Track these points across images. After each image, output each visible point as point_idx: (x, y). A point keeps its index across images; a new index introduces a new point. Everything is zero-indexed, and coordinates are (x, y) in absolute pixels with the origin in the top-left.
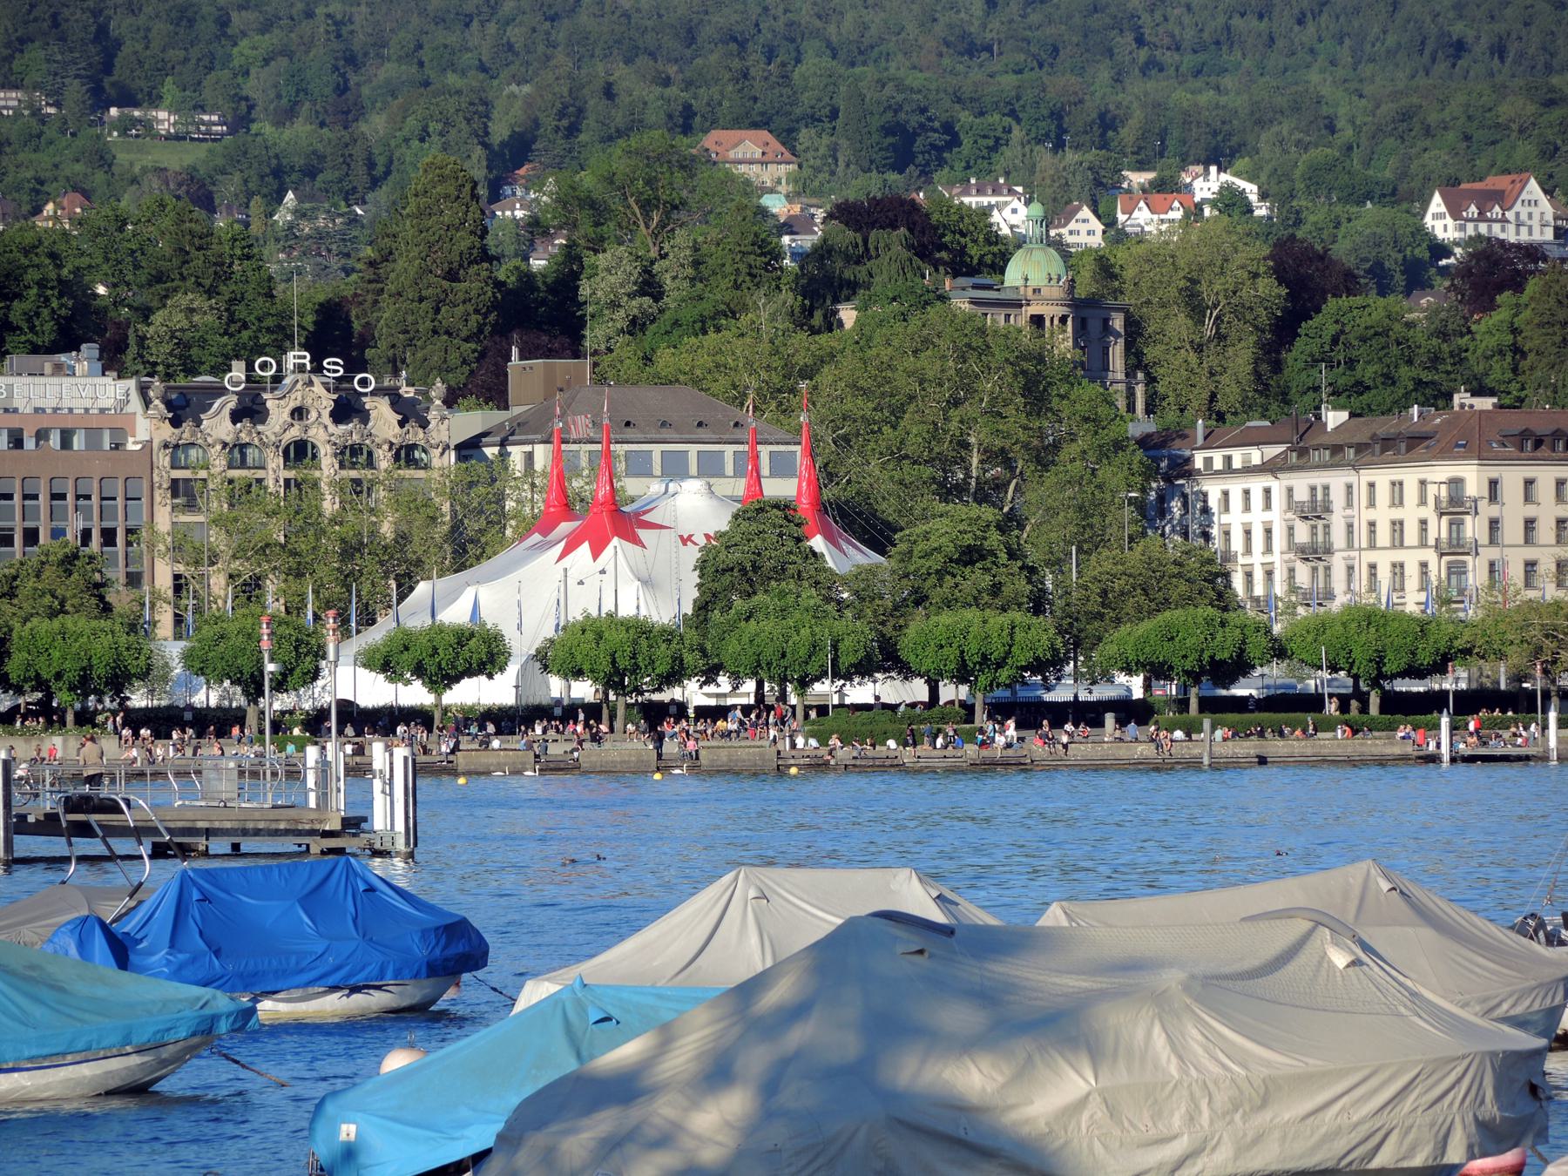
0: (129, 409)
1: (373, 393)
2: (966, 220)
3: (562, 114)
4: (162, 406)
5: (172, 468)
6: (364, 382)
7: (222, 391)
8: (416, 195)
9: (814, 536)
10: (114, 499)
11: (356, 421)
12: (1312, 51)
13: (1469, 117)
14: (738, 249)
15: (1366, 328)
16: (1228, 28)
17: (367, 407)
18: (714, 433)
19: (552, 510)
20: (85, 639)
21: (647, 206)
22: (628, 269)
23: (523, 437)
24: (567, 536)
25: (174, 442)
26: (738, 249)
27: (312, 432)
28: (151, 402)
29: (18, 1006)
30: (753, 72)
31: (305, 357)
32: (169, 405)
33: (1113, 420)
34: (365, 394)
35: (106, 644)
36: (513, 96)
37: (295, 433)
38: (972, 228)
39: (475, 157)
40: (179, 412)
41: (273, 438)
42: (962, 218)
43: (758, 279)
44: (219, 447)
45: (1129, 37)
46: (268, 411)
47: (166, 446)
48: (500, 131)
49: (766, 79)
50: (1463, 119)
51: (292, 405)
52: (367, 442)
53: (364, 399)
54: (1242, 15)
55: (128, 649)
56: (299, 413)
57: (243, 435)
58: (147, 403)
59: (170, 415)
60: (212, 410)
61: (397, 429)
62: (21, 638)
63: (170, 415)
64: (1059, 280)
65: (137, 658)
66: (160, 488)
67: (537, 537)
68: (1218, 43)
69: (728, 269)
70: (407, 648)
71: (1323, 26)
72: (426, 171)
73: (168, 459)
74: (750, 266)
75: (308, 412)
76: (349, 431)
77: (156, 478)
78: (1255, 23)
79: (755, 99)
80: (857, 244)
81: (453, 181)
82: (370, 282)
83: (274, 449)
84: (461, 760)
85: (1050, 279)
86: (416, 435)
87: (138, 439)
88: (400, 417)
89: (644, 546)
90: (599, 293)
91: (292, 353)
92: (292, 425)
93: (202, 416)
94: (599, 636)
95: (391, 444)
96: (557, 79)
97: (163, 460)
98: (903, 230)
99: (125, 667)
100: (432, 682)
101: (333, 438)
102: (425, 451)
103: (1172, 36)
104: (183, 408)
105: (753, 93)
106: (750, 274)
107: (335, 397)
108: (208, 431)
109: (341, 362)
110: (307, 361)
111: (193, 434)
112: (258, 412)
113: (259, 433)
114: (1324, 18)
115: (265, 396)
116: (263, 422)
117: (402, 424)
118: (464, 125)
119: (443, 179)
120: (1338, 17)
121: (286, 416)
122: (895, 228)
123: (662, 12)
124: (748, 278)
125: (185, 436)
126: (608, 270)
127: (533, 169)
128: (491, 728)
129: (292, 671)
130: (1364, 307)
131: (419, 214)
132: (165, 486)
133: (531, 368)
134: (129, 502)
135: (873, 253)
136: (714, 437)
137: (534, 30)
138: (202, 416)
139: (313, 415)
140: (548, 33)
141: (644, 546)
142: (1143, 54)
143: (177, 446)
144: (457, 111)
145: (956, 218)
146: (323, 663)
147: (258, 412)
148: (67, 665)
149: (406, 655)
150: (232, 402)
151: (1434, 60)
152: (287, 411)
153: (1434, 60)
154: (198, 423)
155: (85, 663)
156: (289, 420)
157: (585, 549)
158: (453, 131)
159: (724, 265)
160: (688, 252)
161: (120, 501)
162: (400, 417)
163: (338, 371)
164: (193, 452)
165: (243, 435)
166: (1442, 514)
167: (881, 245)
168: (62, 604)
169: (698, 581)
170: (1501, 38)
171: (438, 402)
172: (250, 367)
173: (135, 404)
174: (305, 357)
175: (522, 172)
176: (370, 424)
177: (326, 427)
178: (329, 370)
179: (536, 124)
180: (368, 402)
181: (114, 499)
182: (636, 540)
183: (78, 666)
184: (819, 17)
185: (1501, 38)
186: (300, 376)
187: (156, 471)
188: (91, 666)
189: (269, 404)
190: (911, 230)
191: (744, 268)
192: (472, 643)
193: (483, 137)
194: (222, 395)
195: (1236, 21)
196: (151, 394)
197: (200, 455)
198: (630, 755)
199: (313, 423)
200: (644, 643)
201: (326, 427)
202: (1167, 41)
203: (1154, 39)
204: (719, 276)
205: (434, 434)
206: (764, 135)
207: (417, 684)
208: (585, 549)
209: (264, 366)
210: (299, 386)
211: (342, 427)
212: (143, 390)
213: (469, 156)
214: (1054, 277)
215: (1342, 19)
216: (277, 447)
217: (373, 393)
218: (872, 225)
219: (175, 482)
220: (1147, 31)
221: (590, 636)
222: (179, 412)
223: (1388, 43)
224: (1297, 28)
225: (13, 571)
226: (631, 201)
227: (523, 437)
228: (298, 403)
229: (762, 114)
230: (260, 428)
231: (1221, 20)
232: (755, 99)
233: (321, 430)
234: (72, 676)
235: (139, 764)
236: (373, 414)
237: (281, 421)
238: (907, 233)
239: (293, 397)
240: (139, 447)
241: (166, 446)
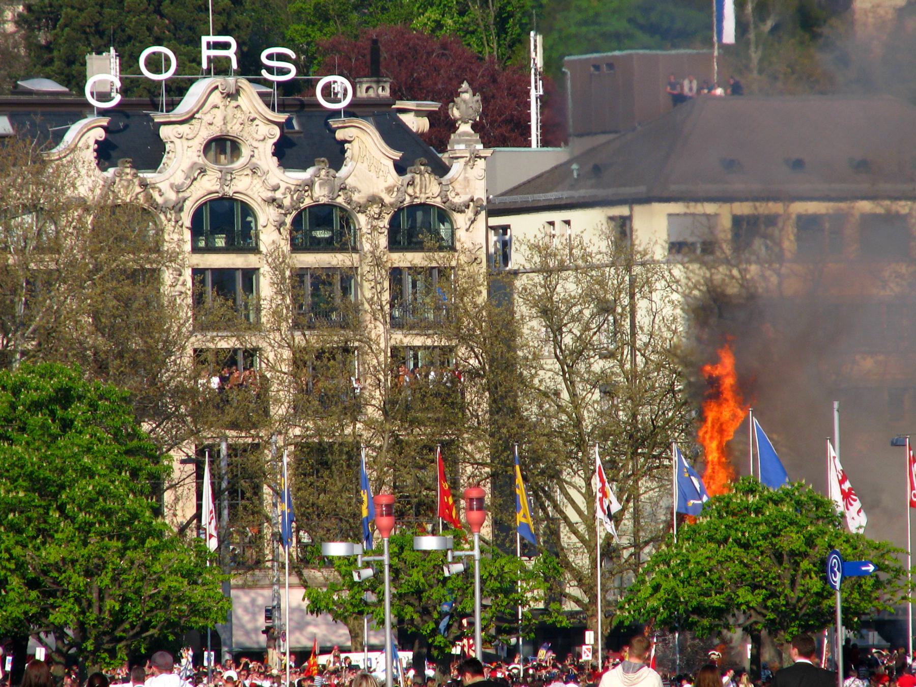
29: (755, 471)
31: (226, 46)
34: (336, 114)
41: (172, 196)
51: (206, 134)
52: (340, 200)
61: (393, 177)
88: (397, 155)
91: (205, 39)
101: (278, 195)
110: (231, 53)
133: (610, 66)
146: (177, 666)
162: (397, 155)
163: (270, 57)
166: (294, 568)
169: (131, 683)
171: (465, 128)
172: (128, 63)
174: (226, 46)
178: (270, 70)
186: (218, 80)
209: (155, 64)
228: (215, 132)
230: (149, 176)
236: (351, 150)
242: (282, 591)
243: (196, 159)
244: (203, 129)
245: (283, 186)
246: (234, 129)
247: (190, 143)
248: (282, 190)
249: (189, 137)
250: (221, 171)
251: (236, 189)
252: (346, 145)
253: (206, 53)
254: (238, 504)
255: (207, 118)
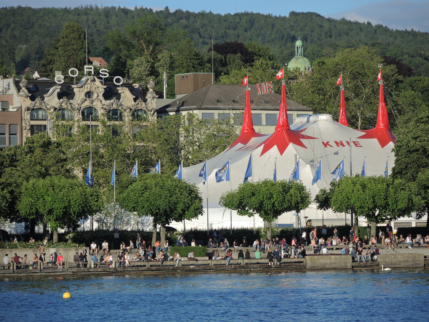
0: (9, 92)
1: (122, 85)
2: (261, 51)
3: (37, 53)
4: (26, 91)
5: (31, 120)
6: (118, 81)
7: (53, 84)
8: (63, 38)
9: (389, 142)
10: (4, 134)
11: (114, 98)
12: (250, 39)
13: (314, 54)
14: (188, 57)
15: (422, 88)
16: (226, 32)
17: (119, 92)
18: (272, 105)
19: (246, 131)
20: (66, 190)
21: (149, 43)
22: (146, 65)
23: (187, 107)
24: (264, 142)
25: (32, 107)
26: (188, 57)
27: (95, 103)
28: (21, 88)
30: (95, 40)
31: (91, 68)
32: (29, 90)
33: (420, 105)
34: (119, 86)
35: (79, 192)
36: (21, 48)
37: (87, 103)
38: (264, 54)
39: (12, 66)
40: (34, 94)
41: (77, 106)
42: (260, 51)
43: (196, 69)
44: (52, 110)
45: (197, 35)
46: (74, 93)
47: (28, 109)
48: (18, 59)
49: (99, 42)
50: (311, 54)
51: (86, 90)
52: (120, 108)
53: (118, 88)
54: (229, 29)
55: (91, 196)
56: (89, 94)
57: (63, 104)
58: (19, 89)
59: (30, 95)
60: (49, 93)
61: (133, 103)
62: (26, 189)
63: (30, 95)
64: (309, 69)
65: (97, 201)
66: (25, 129)
67: (240, 145)
68: (223, 37)
69: (185, 65)
70: (253, 194)
71: (253, 32)
72: (66, 29)
73: (29, 115)
74: (193, 64)
75: (93, 94)
76: (112, 103)
77: (24, 125)
78: (233, 31)
79: (96, 48)
80: (222, 60)
81: (77, 32)
82: (43, 72)
83: (77, 111)
84: (308, 261)
85: (306, 69)
86: (142, 105)
87: (14, 106)
88: (134, 97)
89: (306, 147)
90: (135, 75)
92: (86, 100)
93: (45, 96)
94: (364, 187)
95: (131, 109)
96: (35, 42)
97: (27, 116)
98: (239, 54)
99: (90, 206)
100: (266, 213)
101: (104, 106)
102: (145, 113)
103: (209, 35)
104: (36, 92)
105: (95, 46)
106: (193, 67)
107: (105, 87)
108: (47, 102)
109: (108, 71)
111: (41, 104)
112: (71, 94)
113: (71, 104)
114: (253, 30)
115: (73, 86)
116: (72, 98)
117: (135, 100)
118: (8, 56)
119: (73, 31)
120: (256, 30)
121: (83, 96)
122: (236, 53)
123: (59, 27)
124: (192, 69)
125: (37, 105)
126: (138, 66)
127: (30, 69)
128: (105, 245)
129: (188, 208)
130: (420, 80)
131: (64, 45)
132: (28, 128)
133: (187, 77)
134: (11, 136)
135: (228, 63)
136: (272, 107)
137: (22, 32)
138: (45, 96)
139: (95, 96)
140: (26, 33)
141: (306, 147)
142: (201, 40)
143: (33, 109)
144: (6, 52)
145: (258, 50)
147: (71, 94)
148: (56, 206)
149: (253, 198)
150: (57, 89)
151: (286, 42)
152: (83, 93)
153: (286, 42)
154: (43, 99)
155: (67, 204)
156: (84, 97)
157: (275, 149)
158: (5, 58)
159: (182, 64)
160: (169, 59)
161: (7, 135)
162: (134, 97)
164: (40, 112)
165: (63, 104)
167: (231, 60)
168: (47, 170)
170: (305, 36)
171: (151, 90)
173: (13, 89)
174: (91, 68)
175: (26, 70)
176: (121, 100)
177: (101, 101)
178: (102, 75)
179: (29, 56)
180: (120, 90)
181: (4, 134)
182: (301, 145)
183: (63, 206)
184: (105, 29)
185: (305, 36)
186: (89, 77)
187: (23, 121)
188: (70, 206)
189: (75, 90)
190: (242, 54)
191: (191, 65)
192: (292, 191)
193: (13, 60)
194: (53, 86)
195: (227, 31)
196: (21, 85)
197: (44, 114)
198: (409, 257)
199: (95, 99)
200: (391, 190)
201: (101, 101)
202: (208, 36)
203: (204, 36)
204: (181, 68)
205: (150, 105)
206: (101, 59)
207: (257, 216)
208: (275, 149)
210: (89, 82)
211: (108, 102)
212: (17, 84)
213: (10, 65)
214: (307, 68)
215: (258, 30)
216: (79, 110)
217: (122, 85)
218: (227, 53)
219: (32, 126)
220: (202, 33)
221: (358, 186)
222: (34, 94)
223: (272, 37)
224: (245, 33)
225: (12, 152)
226: (142, 41)
227: (187, 107)
228: (88, 90)
229: (99, 53)
230: (71, 101)
231: (224, 30)
232: (96, 48)
233: (99, 103)
234: (58, 212)
235: (113, 265)
236: (122, 95)
237: (81, 98)
238: (241, 55)
239: (86, 87)
240: (15, 110)
241: (28, 109)
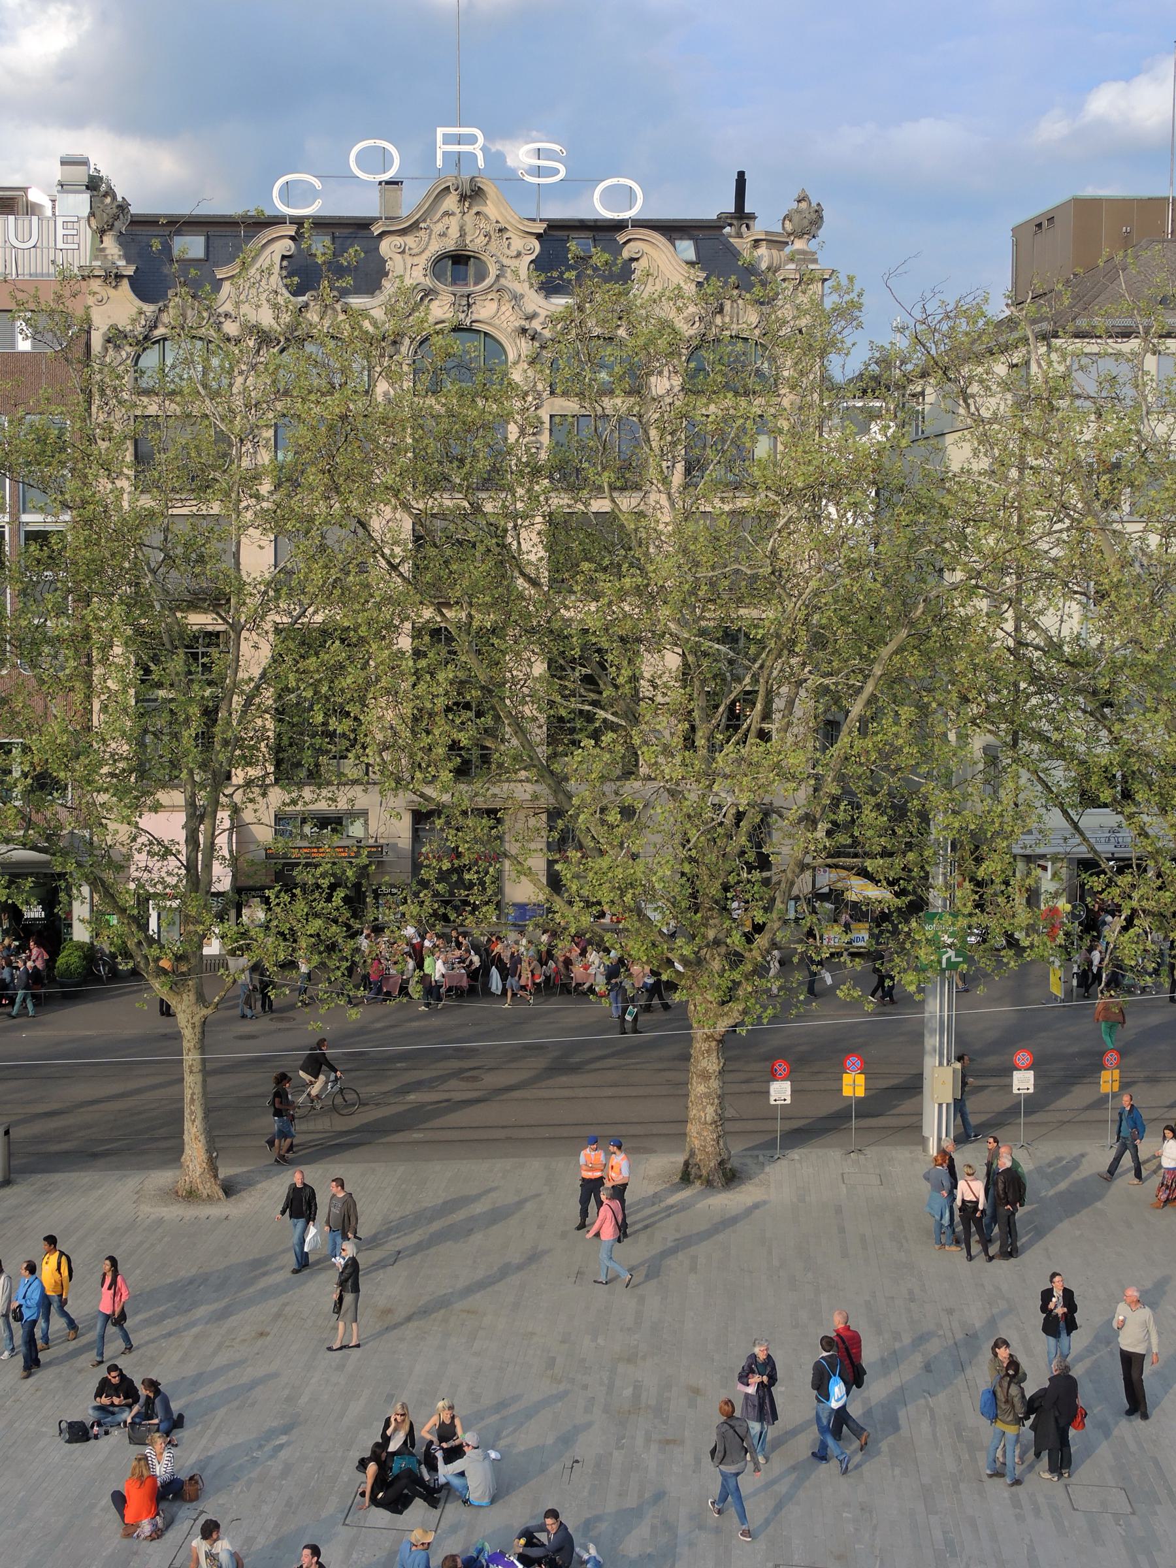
31: (472, 139)
51: (436, 247)
101: (536, 325)
242: (118, 1436)
243: (422, 279)
244: (433, 241)
245: (543, 313)
246: (475, 242)
247: (416, 260)
248: (541, 319)
249: (413, 252)
250: (455, 295)
251: (475, 317)
252: (634, 265)
253: (441, 149)
254: (181, 1061)
255: (439, 228)
